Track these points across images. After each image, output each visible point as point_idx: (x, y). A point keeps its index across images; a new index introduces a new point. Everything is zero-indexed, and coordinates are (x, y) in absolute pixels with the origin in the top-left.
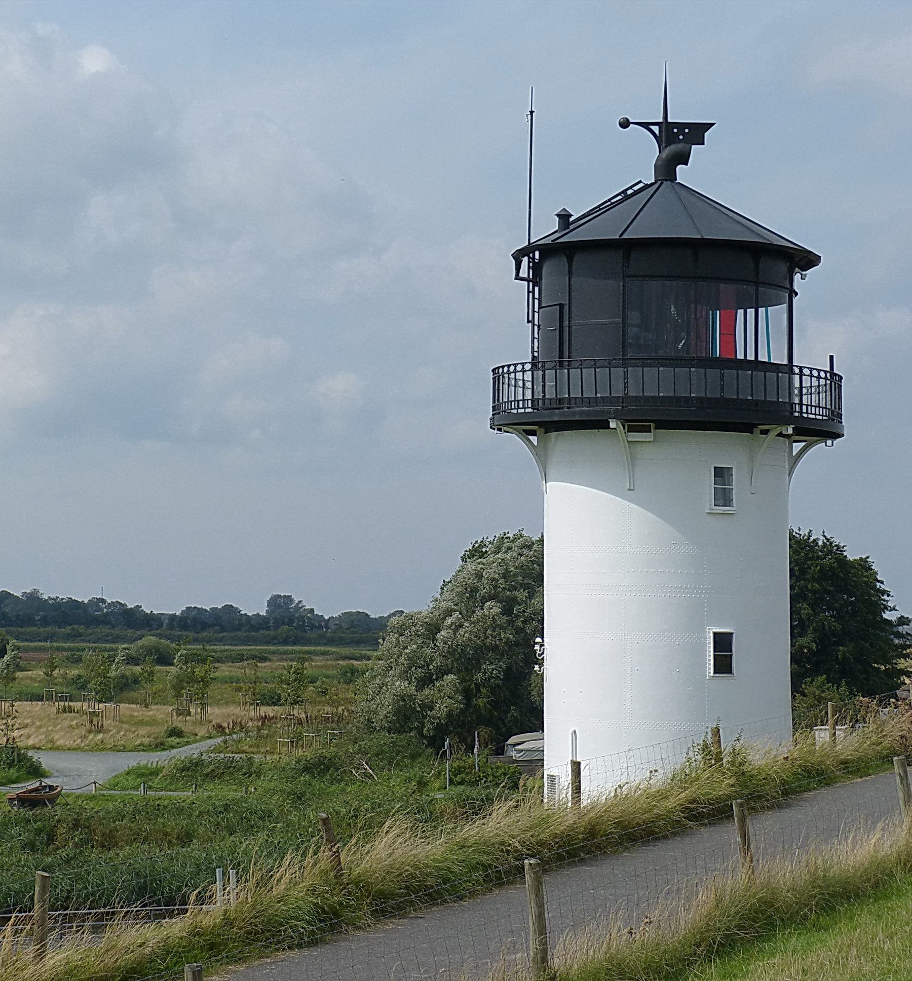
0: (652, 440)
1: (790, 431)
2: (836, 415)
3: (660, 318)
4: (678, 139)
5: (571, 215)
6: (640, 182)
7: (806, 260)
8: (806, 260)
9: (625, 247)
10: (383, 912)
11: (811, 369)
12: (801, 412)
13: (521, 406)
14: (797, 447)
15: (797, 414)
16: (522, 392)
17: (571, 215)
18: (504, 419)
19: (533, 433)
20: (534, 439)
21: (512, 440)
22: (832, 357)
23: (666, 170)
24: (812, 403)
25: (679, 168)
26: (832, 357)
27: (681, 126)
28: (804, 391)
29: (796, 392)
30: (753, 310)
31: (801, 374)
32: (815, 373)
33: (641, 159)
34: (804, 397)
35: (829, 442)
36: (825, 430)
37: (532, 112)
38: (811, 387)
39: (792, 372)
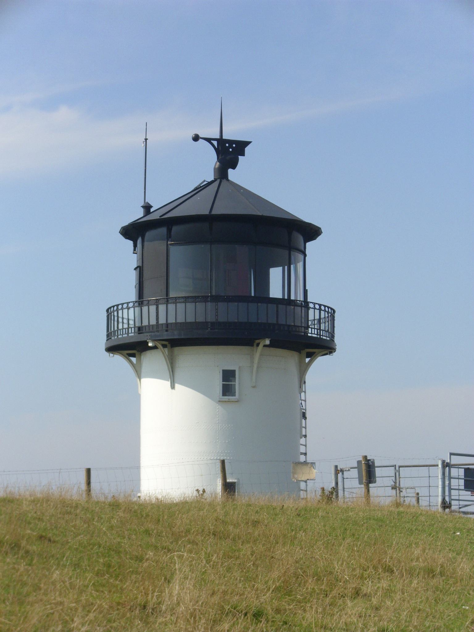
4: (229, 152)
5: (151, 207)
6: (205, 181)
7: (311, 232)
8: (311, 232)
17: (151, 207)
19: (133, 355)
20: (134, 359)
21: (118, 359)
22: (88, 471)
23: (221, 174)
25: (230, 171)
26: (88, 471)
27: (231, 142)
30: (155, 307)
33: (207, 163)
36: (327, 347)
37: (146, 139)
38: (314, 320)
39: (308, 308)
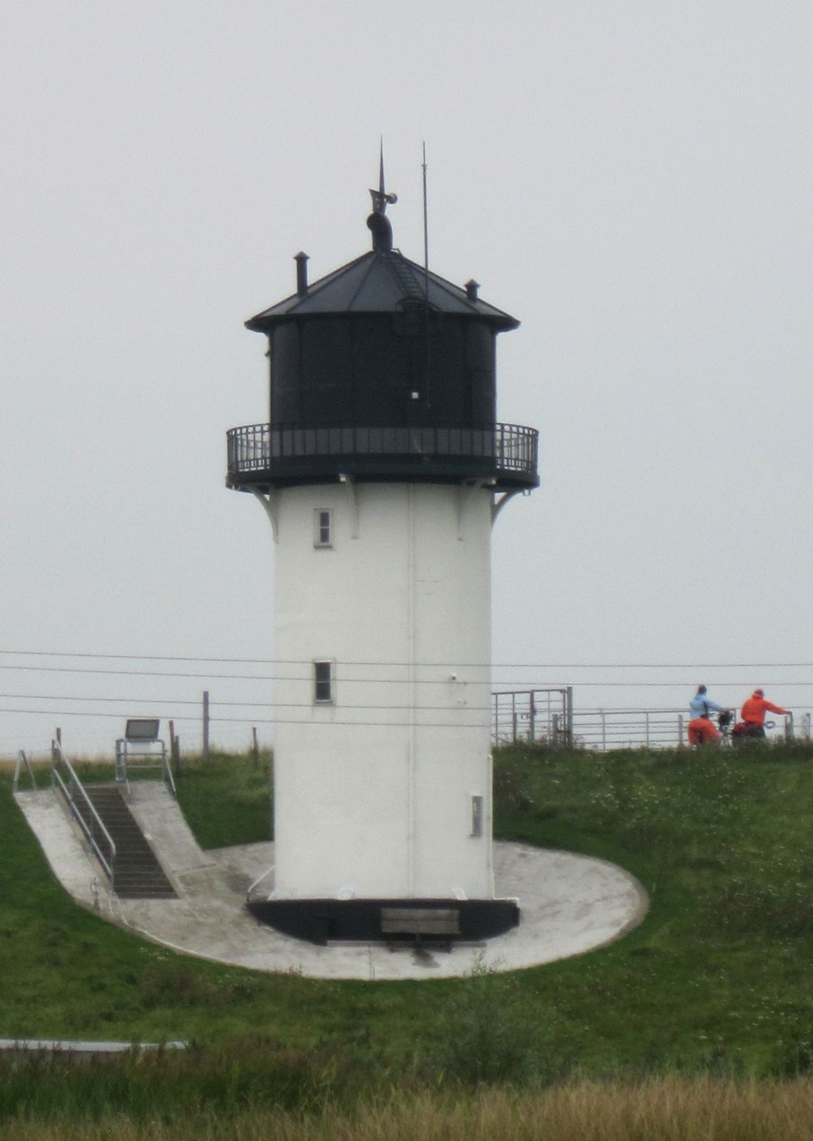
0: (536, 693)
1: (494, 482)
2: (532, 464)
3: (385, 388)
4: (702, 690)
9: (350, 318)
10: (245, 880)
11: (511, 426)
12: (502, 465)
13: (252, 465)
14: (499, 496)
15: (498, 467)
16: (257, 457)
18: (239, 479)
20: (267, 497)
21: (250, 502)
24: (510, 459)
28: (505, 443)
29: (498, 444)
31: (502, 431)
32: (514, 429)
34: (506, 450)
35: (526, 492)
36: (524, 480)
